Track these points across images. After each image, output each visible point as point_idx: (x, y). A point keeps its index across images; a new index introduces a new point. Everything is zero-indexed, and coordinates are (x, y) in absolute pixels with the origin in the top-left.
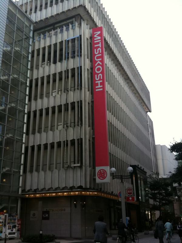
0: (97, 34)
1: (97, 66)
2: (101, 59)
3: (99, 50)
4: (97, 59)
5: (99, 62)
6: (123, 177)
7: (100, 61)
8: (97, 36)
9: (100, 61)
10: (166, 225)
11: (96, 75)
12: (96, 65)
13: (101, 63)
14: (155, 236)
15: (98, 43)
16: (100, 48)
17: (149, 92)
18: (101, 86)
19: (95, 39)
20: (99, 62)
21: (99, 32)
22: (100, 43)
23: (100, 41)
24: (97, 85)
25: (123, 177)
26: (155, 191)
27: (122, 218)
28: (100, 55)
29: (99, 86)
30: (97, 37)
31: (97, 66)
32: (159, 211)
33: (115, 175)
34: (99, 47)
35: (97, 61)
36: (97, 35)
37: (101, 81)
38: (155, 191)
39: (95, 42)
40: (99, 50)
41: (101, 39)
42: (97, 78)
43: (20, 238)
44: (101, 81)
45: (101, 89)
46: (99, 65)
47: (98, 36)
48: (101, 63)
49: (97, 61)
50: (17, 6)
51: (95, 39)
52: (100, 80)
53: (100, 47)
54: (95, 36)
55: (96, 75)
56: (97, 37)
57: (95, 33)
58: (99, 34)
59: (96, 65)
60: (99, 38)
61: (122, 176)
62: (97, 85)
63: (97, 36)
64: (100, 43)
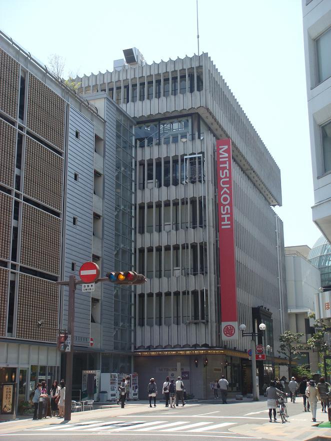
1: (224, 194)
2: (228, 186)
3: (226, 173)
4: (223, 184)
5: (225, 189)
12: (222, 193)
13: (228, 192)
15: (225, 162)
17: (279, 171)
18: (229, 223)
19: (221, 156)
20: (225, 189)
21: (226, 147)
22: (227, 162)
23: (227, 159)
28: (228, 179)
29: (226, 222)
30: (223, 153)
31: (224, 194)
34: (225, 168)
36: (223, 150)
37: (229, 216)
39: (221, 160)
40: (226, 173)
42: (227, 209)
44: (229, 216)
45: (229, 227)
48: (228, 192)
49: (224, 187)
51: (221, 156)
52: (227, 213)
53: (228, 168)
54: (221, 151)
55: (222, 207)
56: (223, 153)
57: (220, 147)
59: (222, 193)
60: (226, 155)
64: (227, 162)
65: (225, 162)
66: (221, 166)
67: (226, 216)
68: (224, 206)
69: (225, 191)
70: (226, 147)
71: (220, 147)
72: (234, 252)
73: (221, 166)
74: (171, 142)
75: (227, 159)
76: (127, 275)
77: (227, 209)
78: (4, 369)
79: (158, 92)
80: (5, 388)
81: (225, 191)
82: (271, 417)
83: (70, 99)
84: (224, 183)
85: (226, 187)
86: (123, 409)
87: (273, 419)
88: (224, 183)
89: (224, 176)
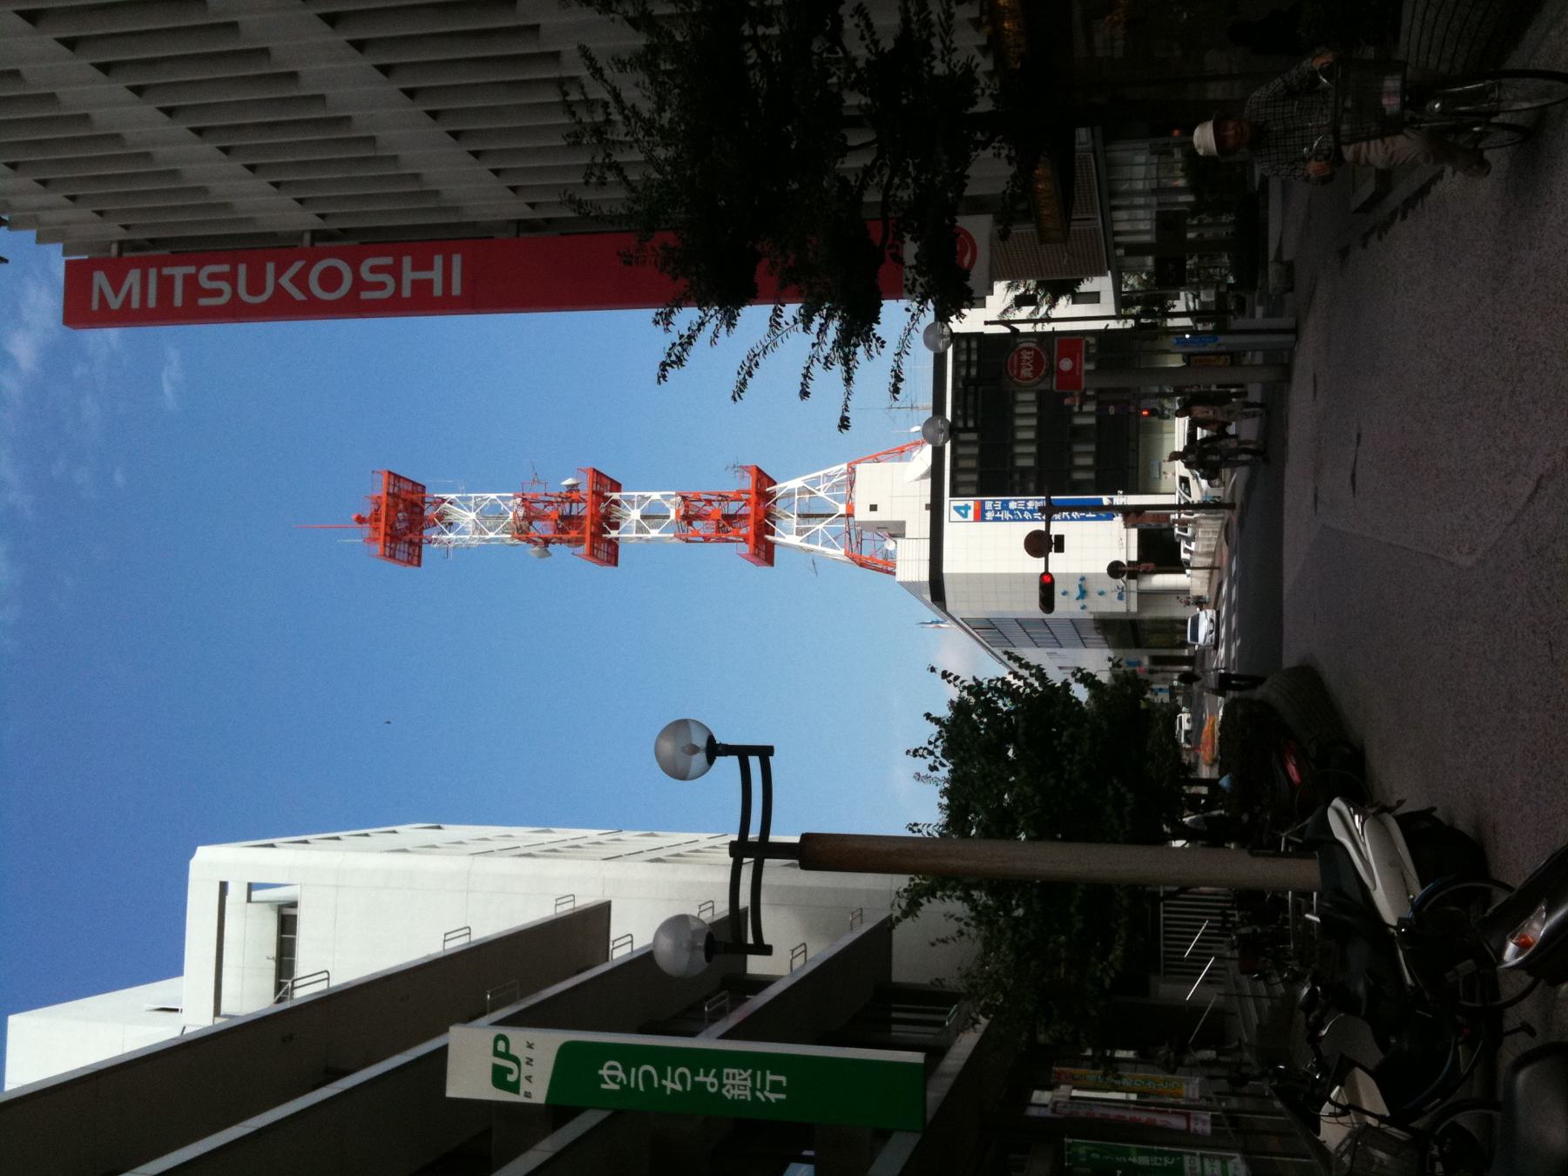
1: (305, 289)
3: (212, 277)
6: (754, 835)
7: (279, 273)
8: (116, 291)
9: (279, 273)
10: (749, 999)
17: (1025, 548)
18: (438, 260)
19: (135, 304)
20: (285, 281)
21: (100, 279)
23: (153, 273)
24: (423, 264)
25: (754, 835)
27: (1124, 494)
29: (436, 275)
31: (305, 289)
33: (1257, 353)
34: (191, 281)
35: (278, 287)
36: (108, 291)
37: (407, 262)
40: (212, 277)
41: (144, 266)
42: (374, 270)
44: (407, 262)
46: (301, 280)
47: (116, 285)
49: (278, 287)
50: (611, 943)
51: (135, 304)
52: (396, 271)
53: (191, 270)
57: (95, 305)
59: (298, 295)
60: (134, 277)
61: (739, 850)
62: (423, 264)
63: (116, 291)
64: (167, 271)
67: (409, 275)
68: (232, 278)
69: (293, 280)
70: (100, 279)
71: (95, 305)
72: (530, 929)
74: (836, 56)
75: (153, 273)
77: (374, 270)
78: (1074, 700)
80: (1470, 961)
81: (293, 280)
84: (166, 284)
85: (278, 275)
88: (166, 284)
89: (225, 286)
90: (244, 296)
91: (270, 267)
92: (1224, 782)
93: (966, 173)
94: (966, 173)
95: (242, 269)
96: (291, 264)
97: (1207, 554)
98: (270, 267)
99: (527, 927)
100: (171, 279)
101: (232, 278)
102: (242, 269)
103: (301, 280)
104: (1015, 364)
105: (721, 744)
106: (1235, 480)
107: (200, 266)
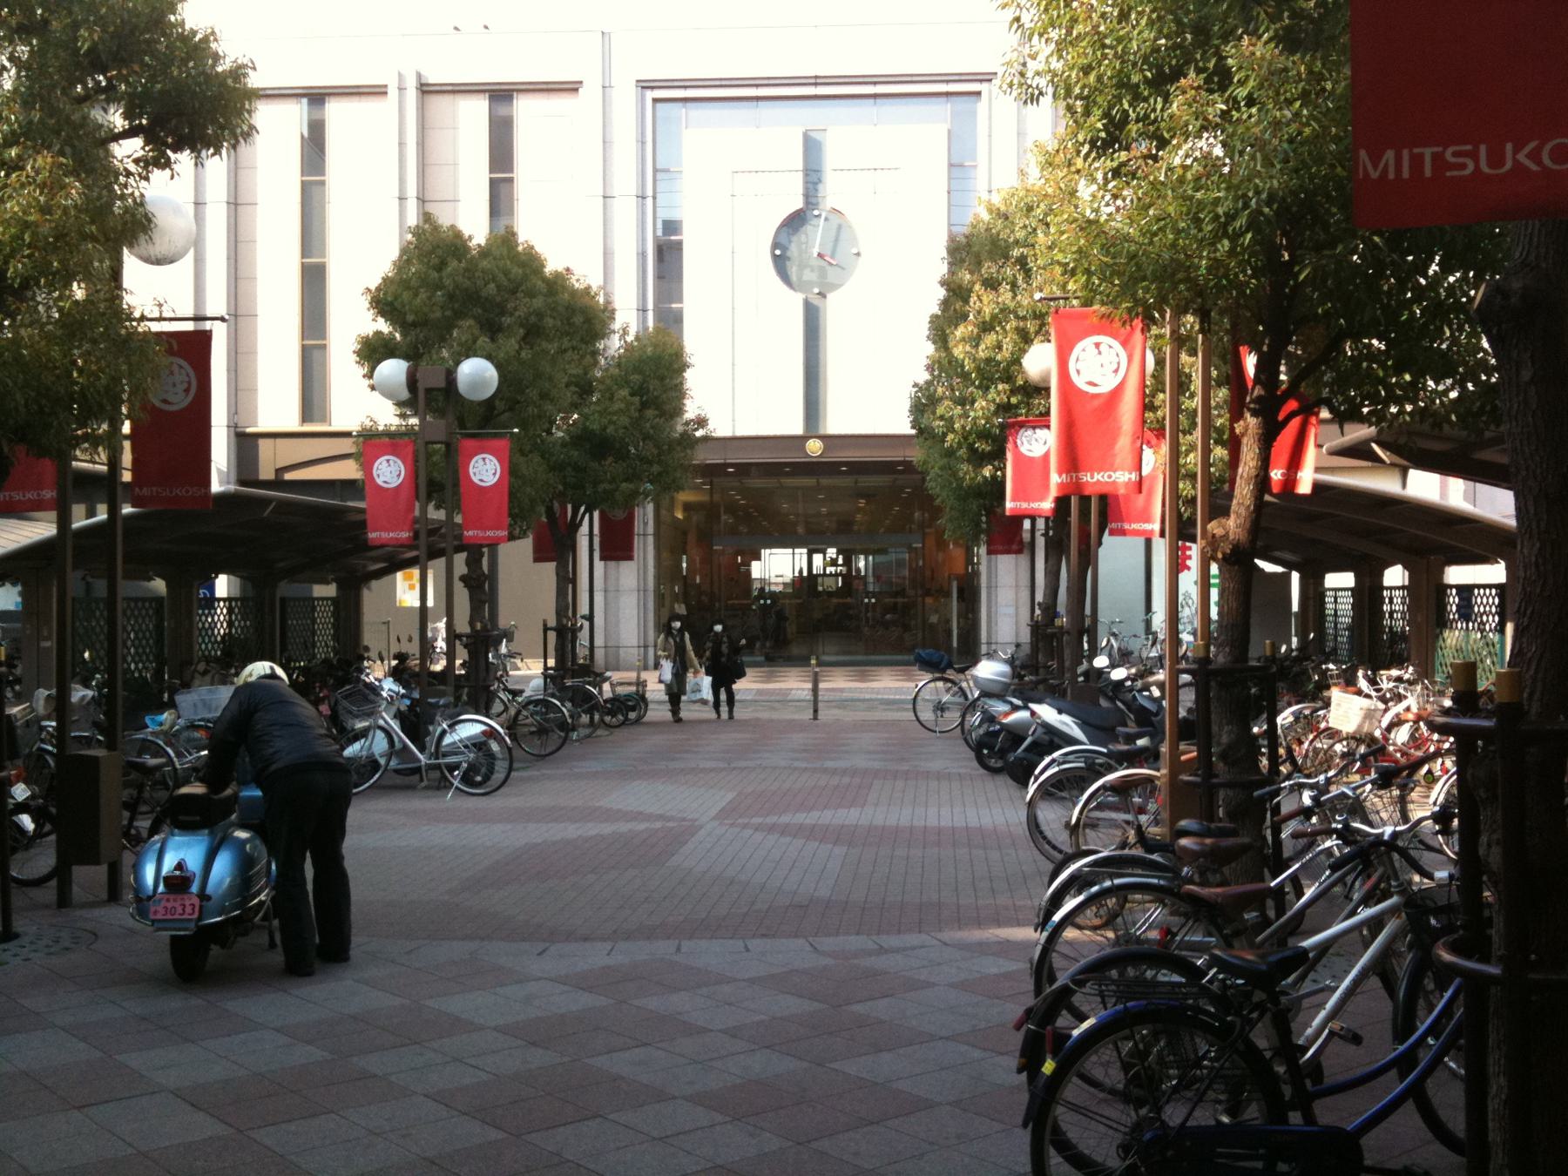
0: (1386, 165)
1: (1539, 162)
4: (1501, 163)
5: (1521, 157)
7: (1516, 151)
8: (1375, 167)
9: (1516, 151)
11: (1468, 147)
12: (1534, 167)
14: (1508, 704)
15: (1417, 161)
16: (1445, 149)
19: (1391, 176)
20: (1521, 157)
22: (1416, 150)
23: (1405, 153)
26: (1126, 1008)
30: (1382, 165)
31: (1539, 162)
32: (357, 815)
34: (1437, 158)
38: (1126, 1008)
39: (1406, 174)
42: (1464, 166)
43: (1023, 667)
49: (1515, 160)
51: (1391, 176)
54: (1375, 175)
55: (1468, 147)
56: (1382, 165)
58: (1370, 159)
59: (1534, 167)
60: (1390, 155)
64: (1416, 150)
65: (1417, 161)
66: (1428, 172)
69: (1528, 156)
73: (1428, 172)
76: (602, 721)
79: (819, 81)
82: (718, 712)
83: (1085, 938)
86: (362, 290)
87: (725, 715)
90: (1486, 169)
91: (1509, 147)
92: (1294, 654)
93: (1025, 1074)
94: (1025, 1074)
95: (1483, 149)
96: (1528, 142)
97: (1365, 800)
98: (1509, 147)
99: (821, 383)
100: (1422, 156)
101: (1474, 156)
102: (1483, 149)
103: (1535, 156)
104: (1311, 602)
105: (923, 405)
106: (1049, 886)
107: (1446, 148)
